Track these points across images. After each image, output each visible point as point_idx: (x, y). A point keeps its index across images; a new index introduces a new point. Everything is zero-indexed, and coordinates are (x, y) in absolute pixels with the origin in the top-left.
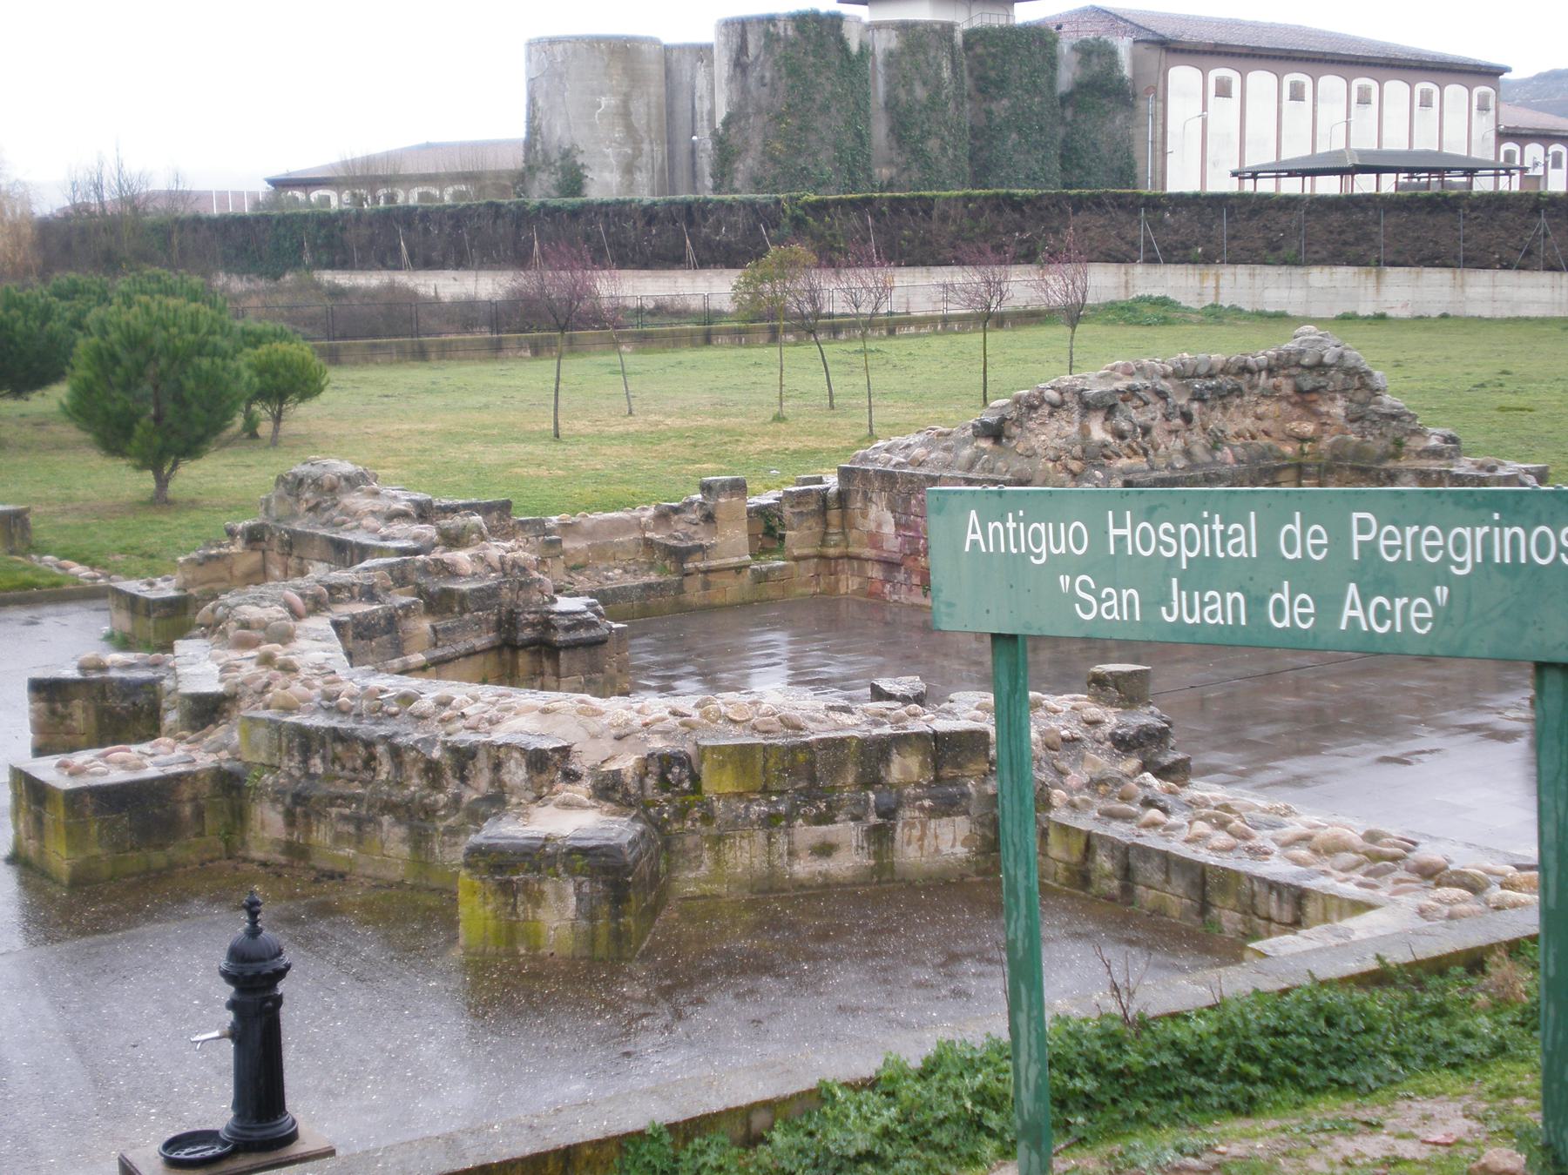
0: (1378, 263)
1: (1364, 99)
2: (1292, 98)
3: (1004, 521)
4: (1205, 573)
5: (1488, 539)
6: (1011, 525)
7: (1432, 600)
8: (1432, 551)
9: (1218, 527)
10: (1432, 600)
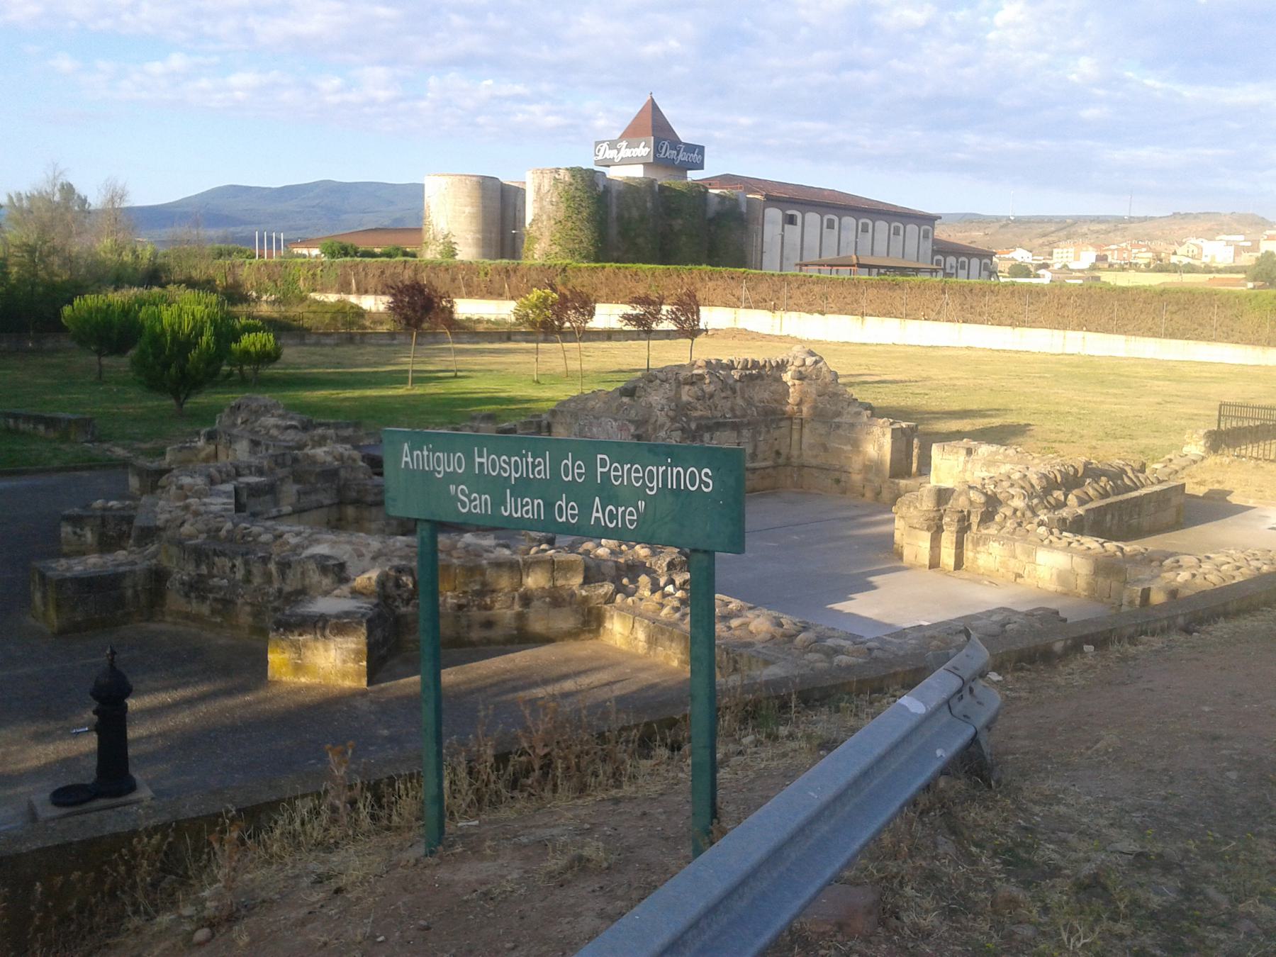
0: (863, 315)
1: (897, 232)
2: (828, 227)
3: (422, 451)
4: (524, 487)
5: (665, 472)
6: (425, 453)
7: (637, 509)
8: (637, 479)
9: (530, 460)
10: (637, 509)
